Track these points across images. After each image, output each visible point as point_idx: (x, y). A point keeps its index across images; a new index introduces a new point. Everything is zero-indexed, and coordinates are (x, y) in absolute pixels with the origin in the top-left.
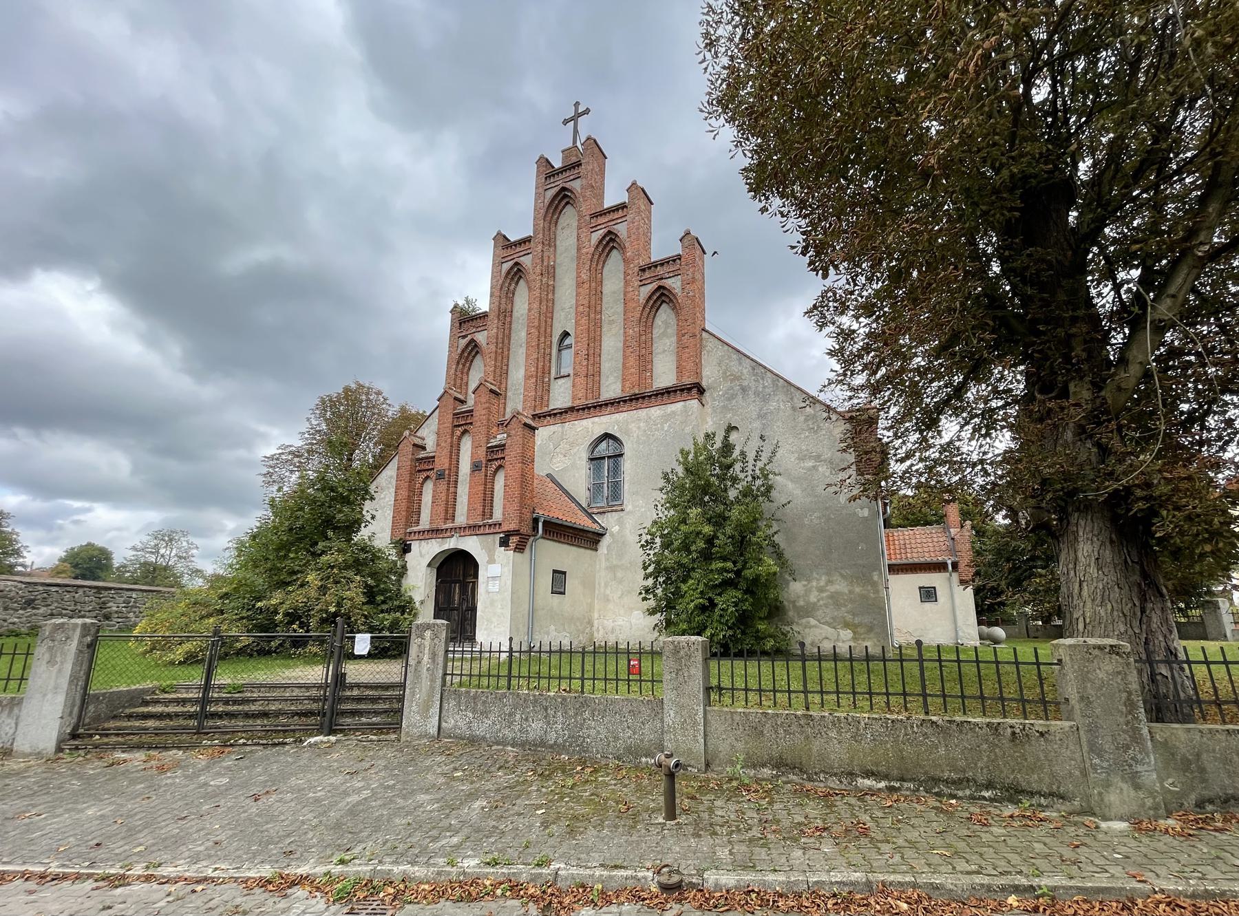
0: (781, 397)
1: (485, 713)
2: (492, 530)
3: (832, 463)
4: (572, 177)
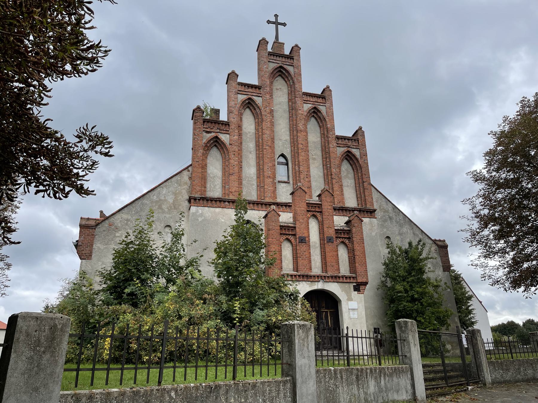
0: (407, 226)
1: (508, 370)
2: (348, 281)
3: (433, 264)
4: (287, 63)
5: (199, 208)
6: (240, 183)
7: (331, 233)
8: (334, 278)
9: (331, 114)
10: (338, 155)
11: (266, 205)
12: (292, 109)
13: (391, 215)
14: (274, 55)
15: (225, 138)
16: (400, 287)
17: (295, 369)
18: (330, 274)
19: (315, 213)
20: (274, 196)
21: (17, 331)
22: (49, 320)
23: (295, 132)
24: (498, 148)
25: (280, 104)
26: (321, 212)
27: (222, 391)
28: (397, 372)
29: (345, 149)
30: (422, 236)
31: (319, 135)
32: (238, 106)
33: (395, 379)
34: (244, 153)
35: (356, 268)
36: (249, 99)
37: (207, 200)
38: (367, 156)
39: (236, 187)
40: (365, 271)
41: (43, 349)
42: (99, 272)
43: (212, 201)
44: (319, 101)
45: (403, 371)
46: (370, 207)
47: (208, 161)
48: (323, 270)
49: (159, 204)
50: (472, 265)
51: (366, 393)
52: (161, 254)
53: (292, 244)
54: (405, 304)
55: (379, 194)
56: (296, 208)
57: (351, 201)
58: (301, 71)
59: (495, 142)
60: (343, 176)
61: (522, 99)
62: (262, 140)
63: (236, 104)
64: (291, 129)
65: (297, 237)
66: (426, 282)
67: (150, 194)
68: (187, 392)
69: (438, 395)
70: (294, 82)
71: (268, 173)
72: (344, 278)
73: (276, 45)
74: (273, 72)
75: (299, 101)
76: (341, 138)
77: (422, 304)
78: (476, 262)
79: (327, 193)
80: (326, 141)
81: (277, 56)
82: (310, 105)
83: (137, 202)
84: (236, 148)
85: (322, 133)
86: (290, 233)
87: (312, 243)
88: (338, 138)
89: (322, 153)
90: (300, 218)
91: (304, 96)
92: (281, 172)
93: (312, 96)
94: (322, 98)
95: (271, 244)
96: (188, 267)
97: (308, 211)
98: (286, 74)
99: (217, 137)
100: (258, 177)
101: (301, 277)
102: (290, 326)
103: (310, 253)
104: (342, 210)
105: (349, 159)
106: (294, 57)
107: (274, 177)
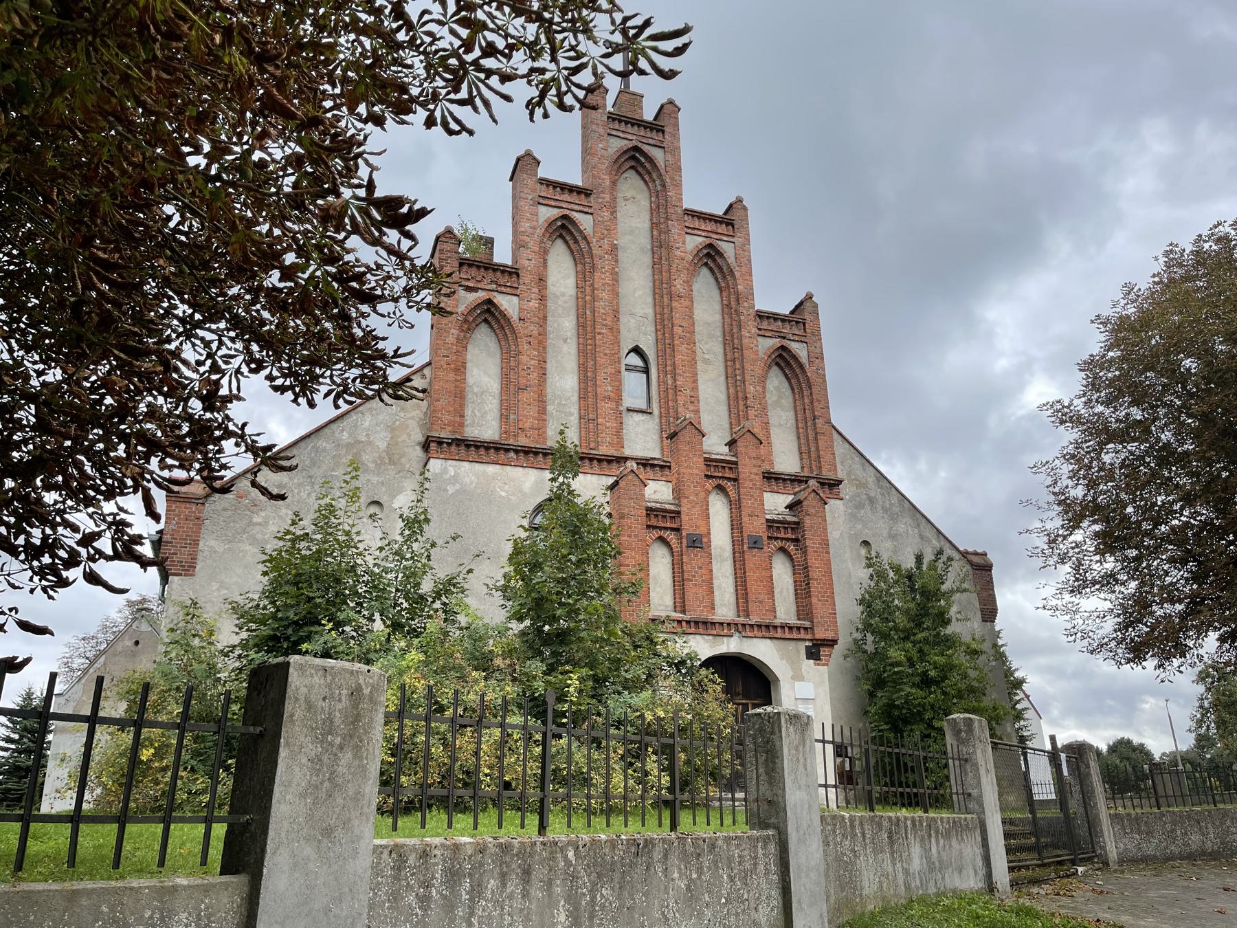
0: (908, 520)
1: (1150, 833)
2: (795, 635)
4: (651, 141)
5: (450, 462)
6: (543, 411)
7: (756, 527)
8: (763, 628)
9: (745, 260)
10: (761, 354)
11: (600, 461)
12: (660, 247)
13: (872, 494)
14: (620, 121)
15: (508, 304)
16: (899, 652)
17: (785, 810)
18: (754, 619)
19: (723, 483)
20: (618, 443)
21: (290, 698)
22: (348, 676)
23: (666, 299)
24: (1111, 354)
25: (632, 232)
26: (735, 480)
27: (657, 854)
28: (957, 828)
29: (776, 342)
30: (939, 541)
31: (718, 307)
32: (540, 231)
33: (954, 842)
34: (551, 340)
35: (811, 608)
36: (565, 217)
37: (468, 446)
38: (823, 359)
39: (534, 418)
40: (831, 614)
41: (338, 741)
42: (231, 604)
43: (477, 447)
44: (720, 231)
45: (967, 826)
46: (828, 473)
47: (469, 357)
48: (738, 611)
49: (355, 451)
50: (1044, 608)
51: (906, 872)
52: (375, 565)
53: (671, 549)
54: (909, 690)
55: (847, 445)
56: (682, 470)
57: (787, 460)
58: (679, 160)
59: (1104, 339)
60: (769, 402)
61: (1168, 249)
62: (593, 312)
63: (534, 228)
64: (657, 291)
65: (684, 533)
66: (954, 643)
67: (333, 426)
68: (595, 853)
69: (1029, 882)
70: (664, 185)
71: (606, 388)
72: (786, 629)
73: (624, 97)
74: (618, 158)
75: (675, 229)
76: (768, 318)
77: (945, 693)
78: (1054, 602)
79: (748, 436)
80: (734, 323)
81: (627, 123)
82: (701, 239)
83: (302, 444)
84: (533, 329)
85: (725, 302)
86: (668, 525)
87: (715, 549)
88: (761, 316)
89: (725, 349)
90: (689, 491)
91: (686, 218)
92: (634, 388)
93: (704, 219)
94: (727, 224)
95: (626, 548)
96: (438, 595)
97: (706, 476)
98: (648, 165)
99: (489, 302)
100: (583, 397)
101: (692, 624)
102: (769, 717)
103: (711, 571)
104: (773, 479)
105: (783, 364)
106: (665, 128)
107: (619, 400)
